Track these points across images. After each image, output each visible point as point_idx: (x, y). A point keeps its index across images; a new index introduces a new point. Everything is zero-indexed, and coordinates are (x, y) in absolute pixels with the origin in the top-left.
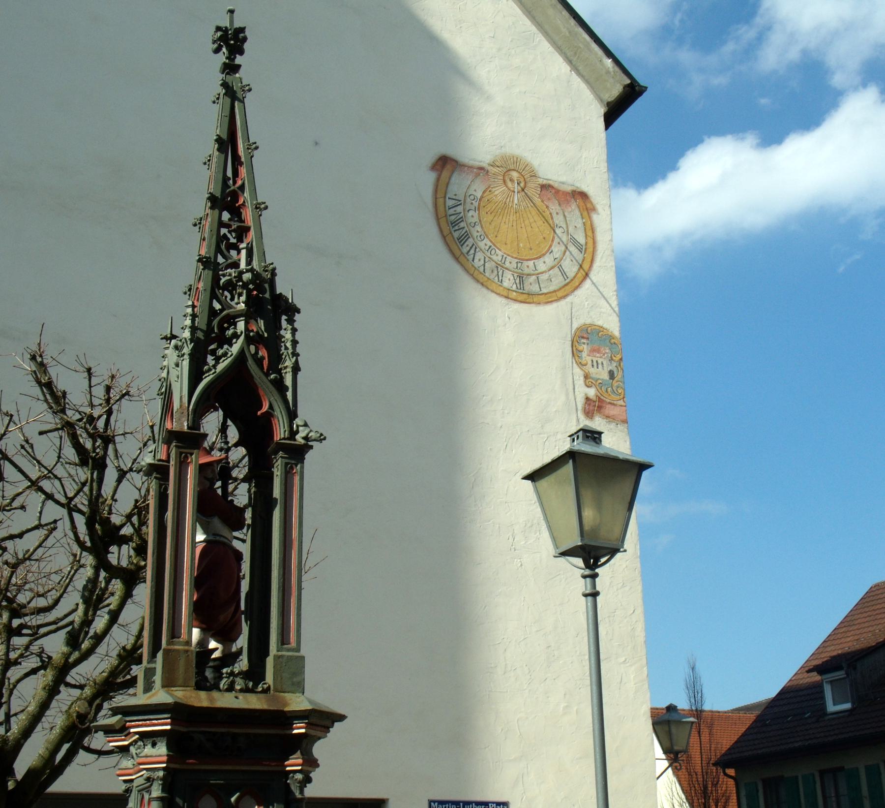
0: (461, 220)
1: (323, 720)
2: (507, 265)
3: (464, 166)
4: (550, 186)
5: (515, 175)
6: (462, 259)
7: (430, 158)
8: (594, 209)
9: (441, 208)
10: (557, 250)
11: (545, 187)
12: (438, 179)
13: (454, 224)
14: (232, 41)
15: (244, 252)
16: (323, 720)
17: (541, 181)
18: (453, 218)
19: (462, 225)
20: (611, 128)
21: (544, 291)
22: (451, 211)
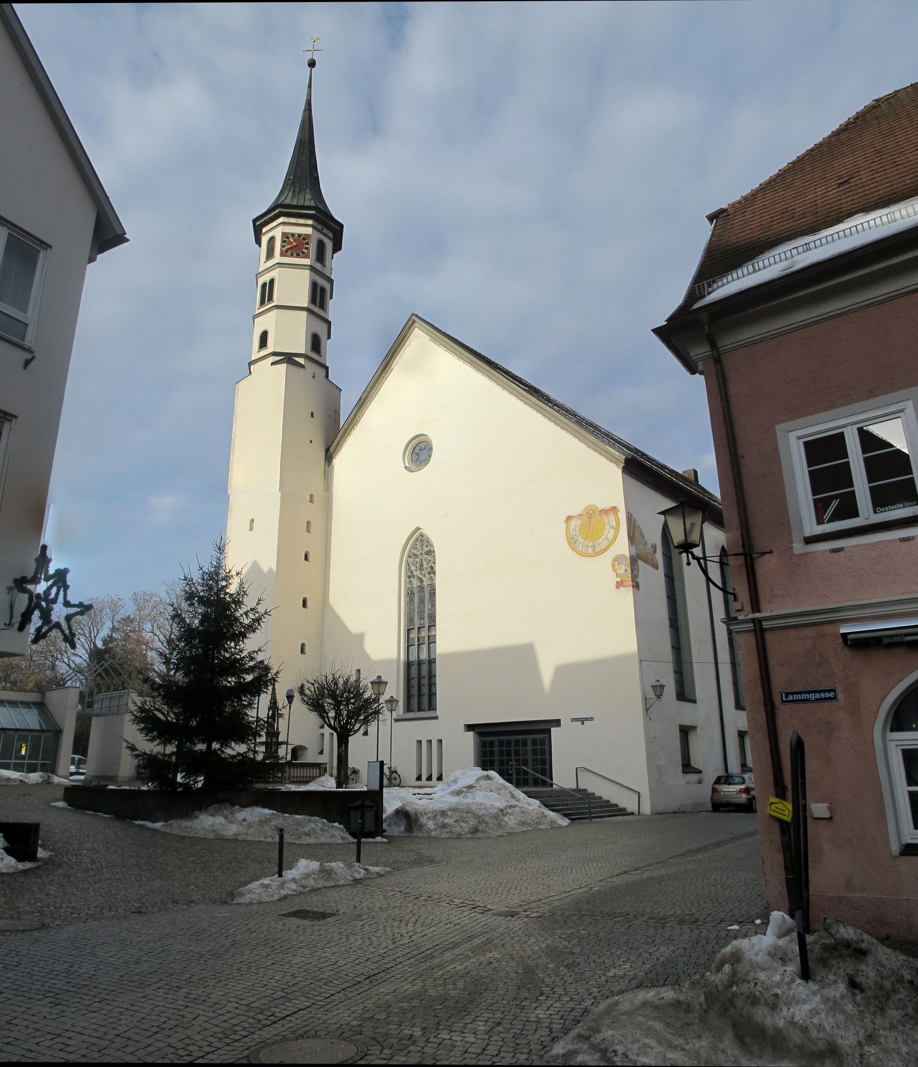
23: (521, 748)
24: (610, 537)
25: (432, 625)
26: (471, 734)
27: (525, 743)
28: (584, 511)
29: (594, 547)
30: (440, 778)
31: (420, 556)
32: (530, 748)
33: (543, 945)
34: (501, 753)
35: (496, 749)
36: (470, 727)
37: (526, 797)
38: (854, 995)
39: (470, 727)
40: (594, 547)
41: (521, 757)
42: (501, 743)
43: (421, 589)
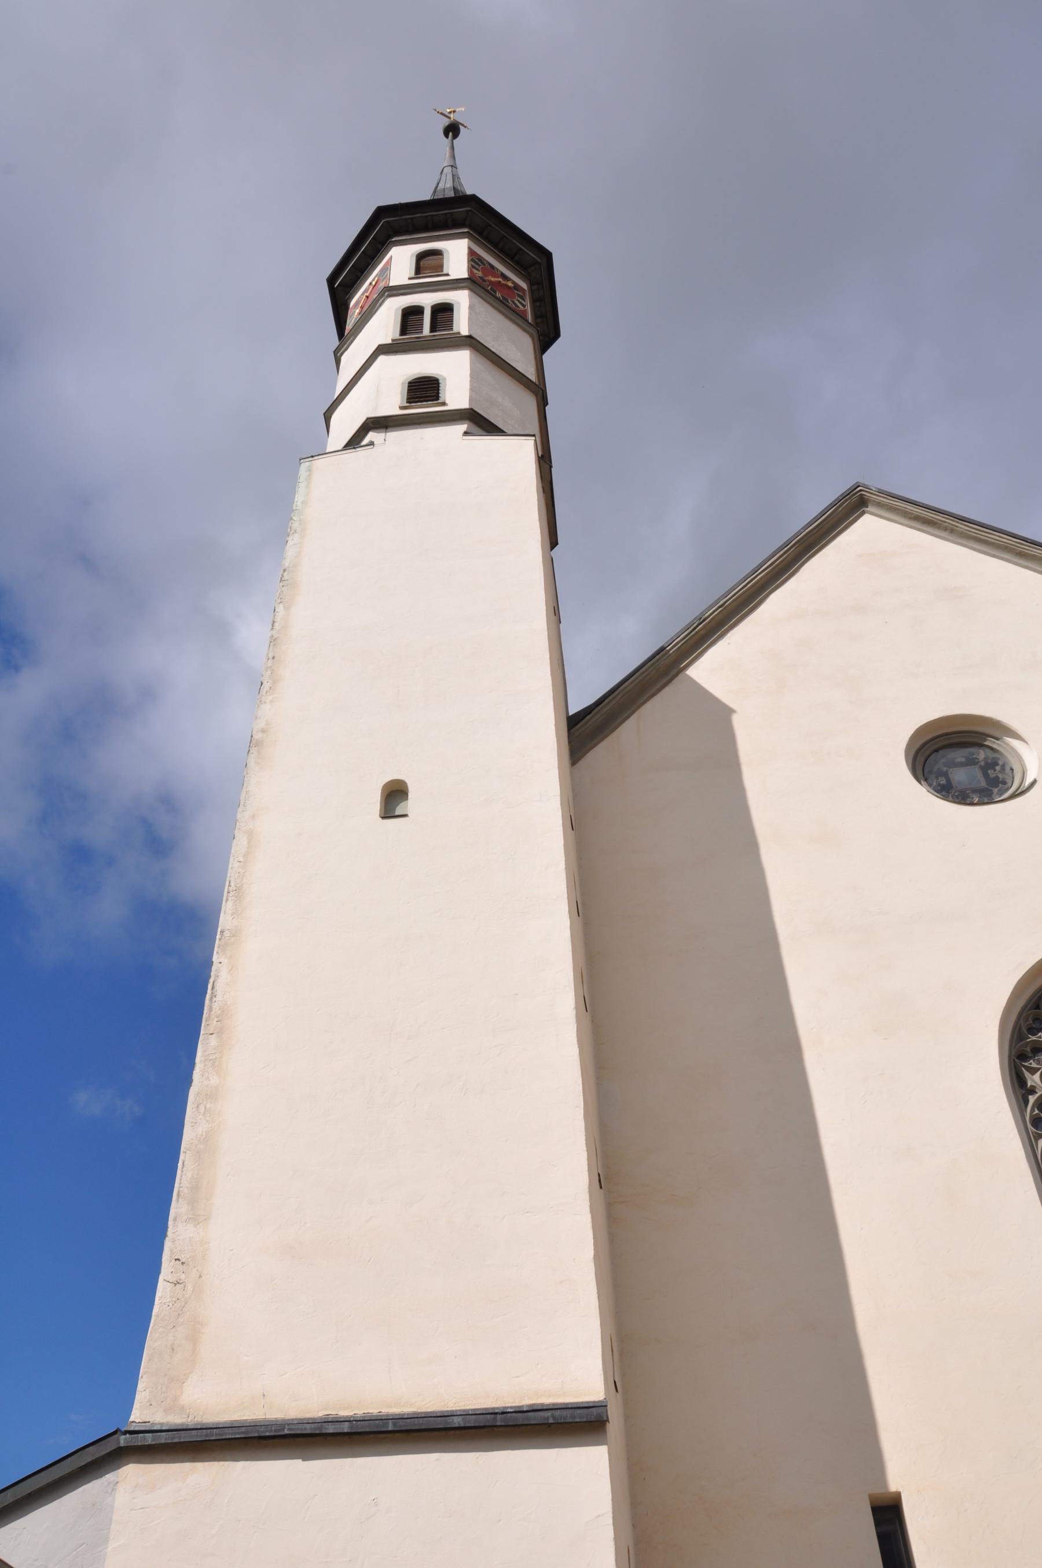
12: (879, 505)
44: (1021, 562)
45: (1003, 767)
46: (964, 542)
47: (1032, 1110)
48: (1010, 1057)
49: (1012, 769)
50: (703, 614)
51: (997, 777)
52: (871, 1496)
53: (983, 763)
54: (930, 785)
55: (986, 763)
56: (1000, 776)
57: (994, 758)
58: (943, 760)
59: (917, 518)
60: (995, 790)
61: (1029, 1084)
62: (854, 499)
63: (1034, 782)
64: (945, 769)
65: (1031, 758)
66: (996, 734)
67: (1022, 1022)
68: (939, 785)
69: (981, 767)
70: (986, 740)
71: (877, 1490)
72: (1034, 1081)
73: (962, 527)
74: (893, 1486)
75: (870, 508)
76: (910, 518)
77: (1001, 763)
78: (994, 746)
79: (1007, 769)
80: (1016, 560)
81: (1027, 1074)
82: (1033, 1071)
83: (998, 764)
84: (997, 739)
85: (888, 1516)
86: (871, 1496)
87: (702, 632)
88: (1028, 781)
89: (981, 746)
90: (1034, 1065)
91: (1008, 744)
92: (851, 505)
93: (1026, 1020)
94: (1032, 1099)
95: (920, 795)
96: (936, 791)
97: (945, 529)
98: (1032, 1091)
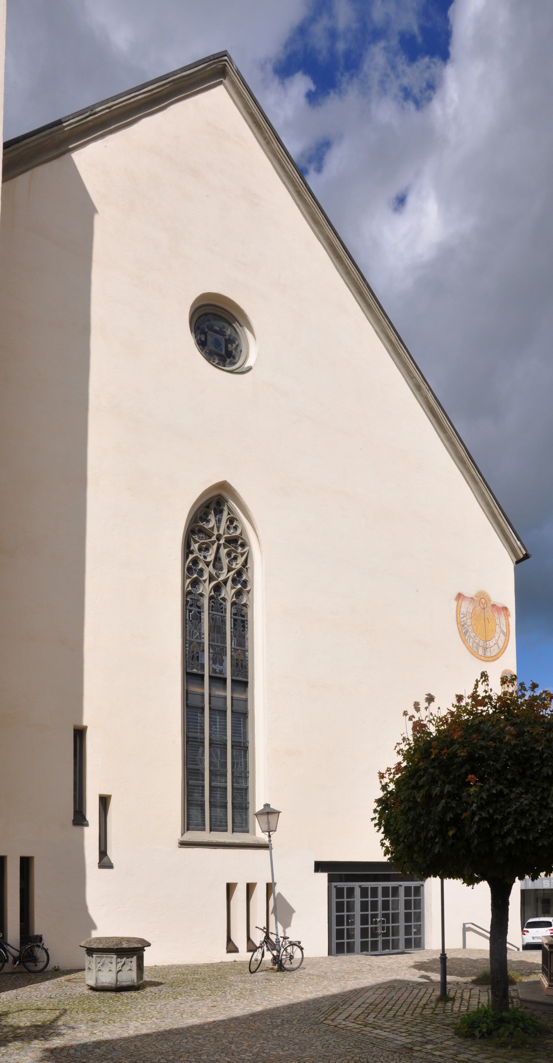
0: (465, 624)
1: (463, 883)
2: (480, 644)
3: (466, 597)
4: (495, 605)
5: (483, 600)
6: (466, 642)
7: (455, 595)
8: (509, 615)
9: (459, 619)
10: (497, 635)
11: (494, 606)
12: (233, 83)
13: (463, 626)
14: (257, 927)
15: (420, 1048)
16: (463, 883)
17: (492, 603)
18: (462, 623)
19: (466, 626)
20: (8, 182)
21: (492, 655)
22: (462, 620)
23: (390, 898)
24: (501, 644)
25: (242, 683)
26: (324, 876)
27: (395, 891)
28: (476, 596)
29: (485, 649)
30: (230, 888)
31: (213, 526)
32: (402, 897)
33: (283, 957)
34: (364, 906)
35: (357, 899)
36: (320, 866)
37: (417, 971)
38: (406, 966)
39: (320, 866)
40: (485, 649)
41: (391, 912)
42: (364, 892)
43: (217, 604)
44: (297, 199)
45: (237, 346)
46: (272, 158)
47: (189, 563)
48: (188, 529)
49: (241, 351)
50: (94, 106)
51: (232, 352)
52: (100, 795)
53: (227, 337)
54: (196, 337)
55: (229, 338)
56: (234, 352)
57: (234, 337)
58: (207, 323)
59: (251, 115)
60: (228, 360)
61: (192, 548)
62: (220, 65)
63: (250, 369)
64: (207, 330)
65: (254, 350)
66: (242, 323)
67: (199, 512)
68: (200, 339)
69: (226, 339)
70: (234, 323)
71: (78, 724)
72: (194, 547)
73: (275, 145)
74: (85, 724)
75: (226, 82)
76: (248, 112)
77: (237, 343)
78: (237, 330)
79: (239, 350)
80: (294, 195)
81: (192, 542)
82: (196, 542)
83: (235, 343)
84: (241, 326)
85: (80, 734)
86: (100, 795)
87: (91, 124)
88: (247, 365)
89: (231, 325)
90: (197, 539)
91: (245, 333)
92: (212, 71)
93: (201, 513)
94: (191, 557)
95: (188, 340)
96: (198, 343)
97: (265, 138)
98: (192, 552)
